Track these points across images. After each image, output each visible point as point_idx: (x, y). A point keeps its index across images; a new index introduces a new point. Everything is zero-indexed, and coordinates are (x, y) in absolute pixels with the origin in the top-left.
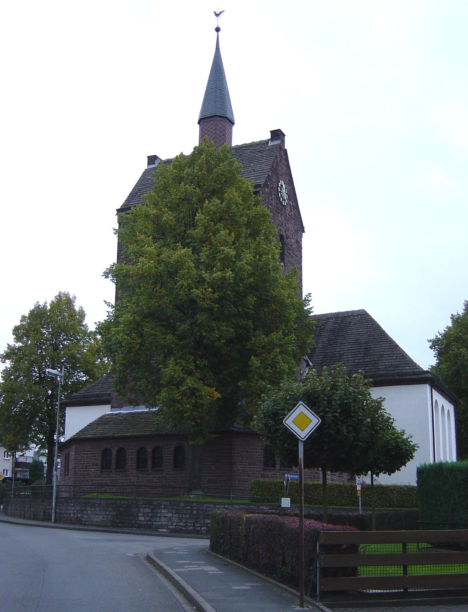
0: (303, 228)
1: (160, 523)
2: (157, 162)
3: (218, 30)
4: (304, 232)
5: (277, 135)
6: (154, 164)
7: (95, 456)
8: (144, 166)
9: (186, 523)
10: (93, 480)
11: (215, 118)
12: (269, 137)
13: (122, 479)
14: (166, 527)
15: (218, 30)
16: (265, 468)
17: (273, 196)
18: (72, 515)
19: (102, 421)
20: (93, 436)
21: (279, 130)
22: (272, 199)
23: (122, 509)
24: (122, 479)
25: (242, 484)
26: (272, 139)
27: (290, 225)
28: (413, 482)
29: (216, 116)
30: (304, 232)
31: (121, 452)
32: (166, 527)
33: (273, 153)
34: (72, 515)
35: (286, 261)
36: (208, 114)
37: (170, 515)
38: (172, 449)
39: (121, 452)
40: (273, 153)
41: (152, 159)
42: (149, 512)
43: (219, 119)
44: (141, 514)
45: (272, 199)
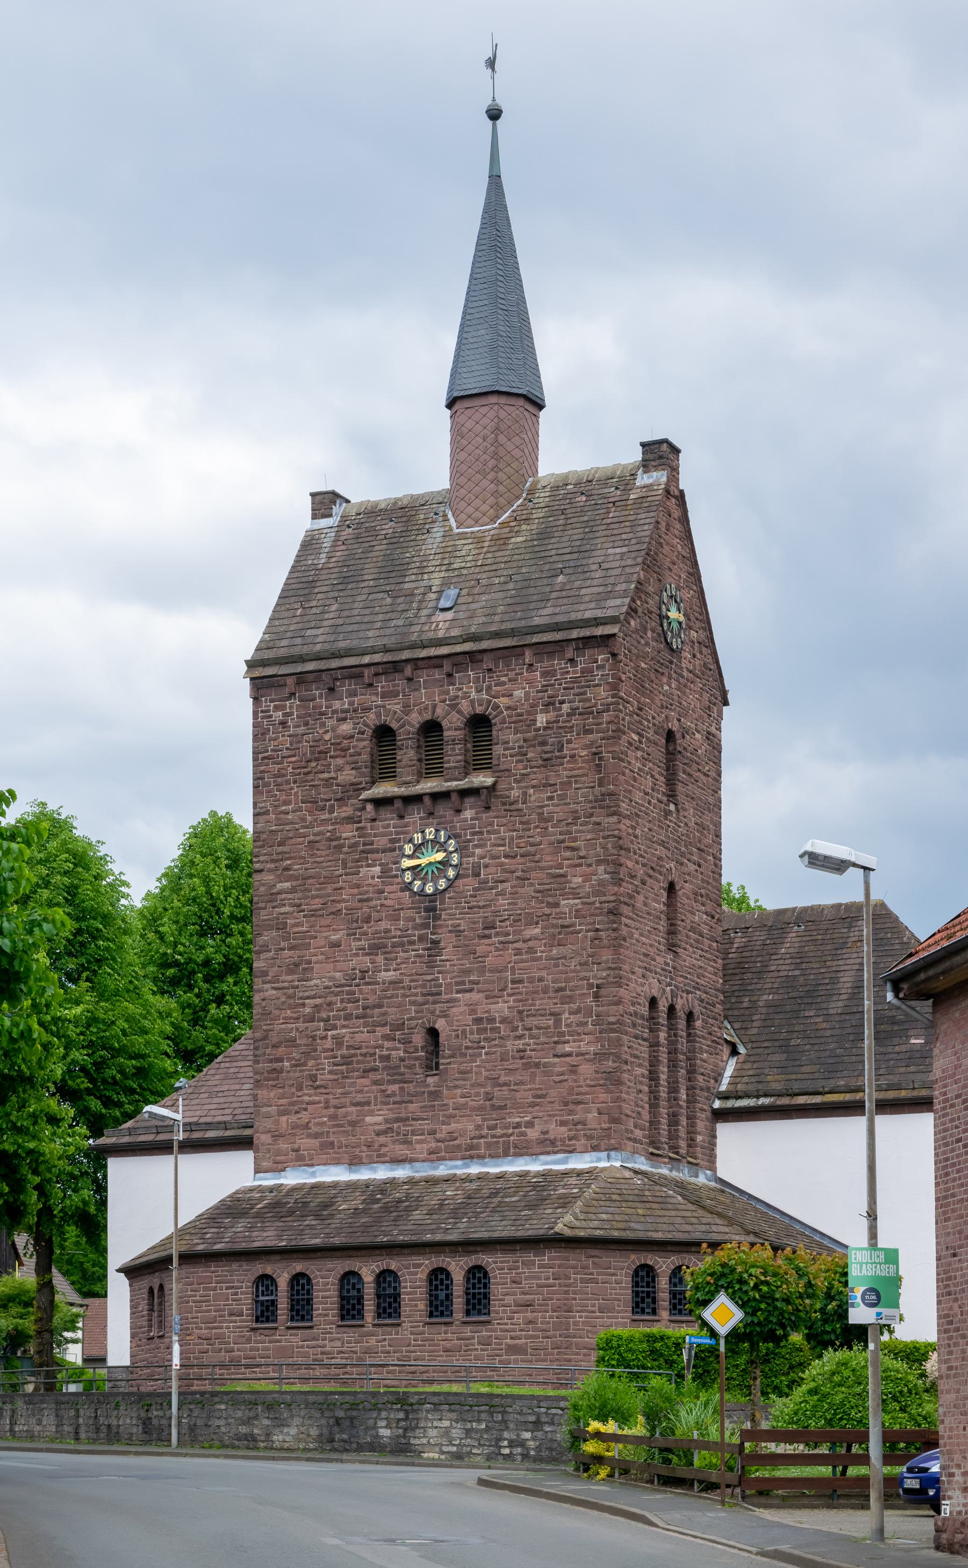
0: (724, 693)
1: (424, 1441)
2: (338, 510)
3: (494, 114)
4: (726, 703)
5: (661, 453)
6: (330, 516)
7: (236, 1294)
8: (301, 521)
9: (479, 1440)
10: (232, 1351)
11: (493, 399)
12: (637, 455)
13: (302, 1347)
14: (437, 1449)
15: (494, 114)
16: (636, 1317)
17: (649, 634)
18: (223, 1429)
19: (233, 1208)
20: (229, 1245)
21: (666, 441)
22: (647, 644)
23: (341, 1414)
24: (302, 1347)
25: (585, 1355)
26: (646, 465)
27: (692, 699)
28: (611, 1422)
29: (496, 391)
30: (726, 703)
31: (300, 1283)
32: (437, 1449)
33: (647, 510)
34: (223, 1429)
35: (681, 798)
36: (472, 385)
37: (446, 1423)
38: (424, 1276)
39: (300, 1283)
40: (647, 510)
41: (324, 502)
42: (401, 1419)
43: (503, 400)
44: (384, 1423)
45: (647, 644)
